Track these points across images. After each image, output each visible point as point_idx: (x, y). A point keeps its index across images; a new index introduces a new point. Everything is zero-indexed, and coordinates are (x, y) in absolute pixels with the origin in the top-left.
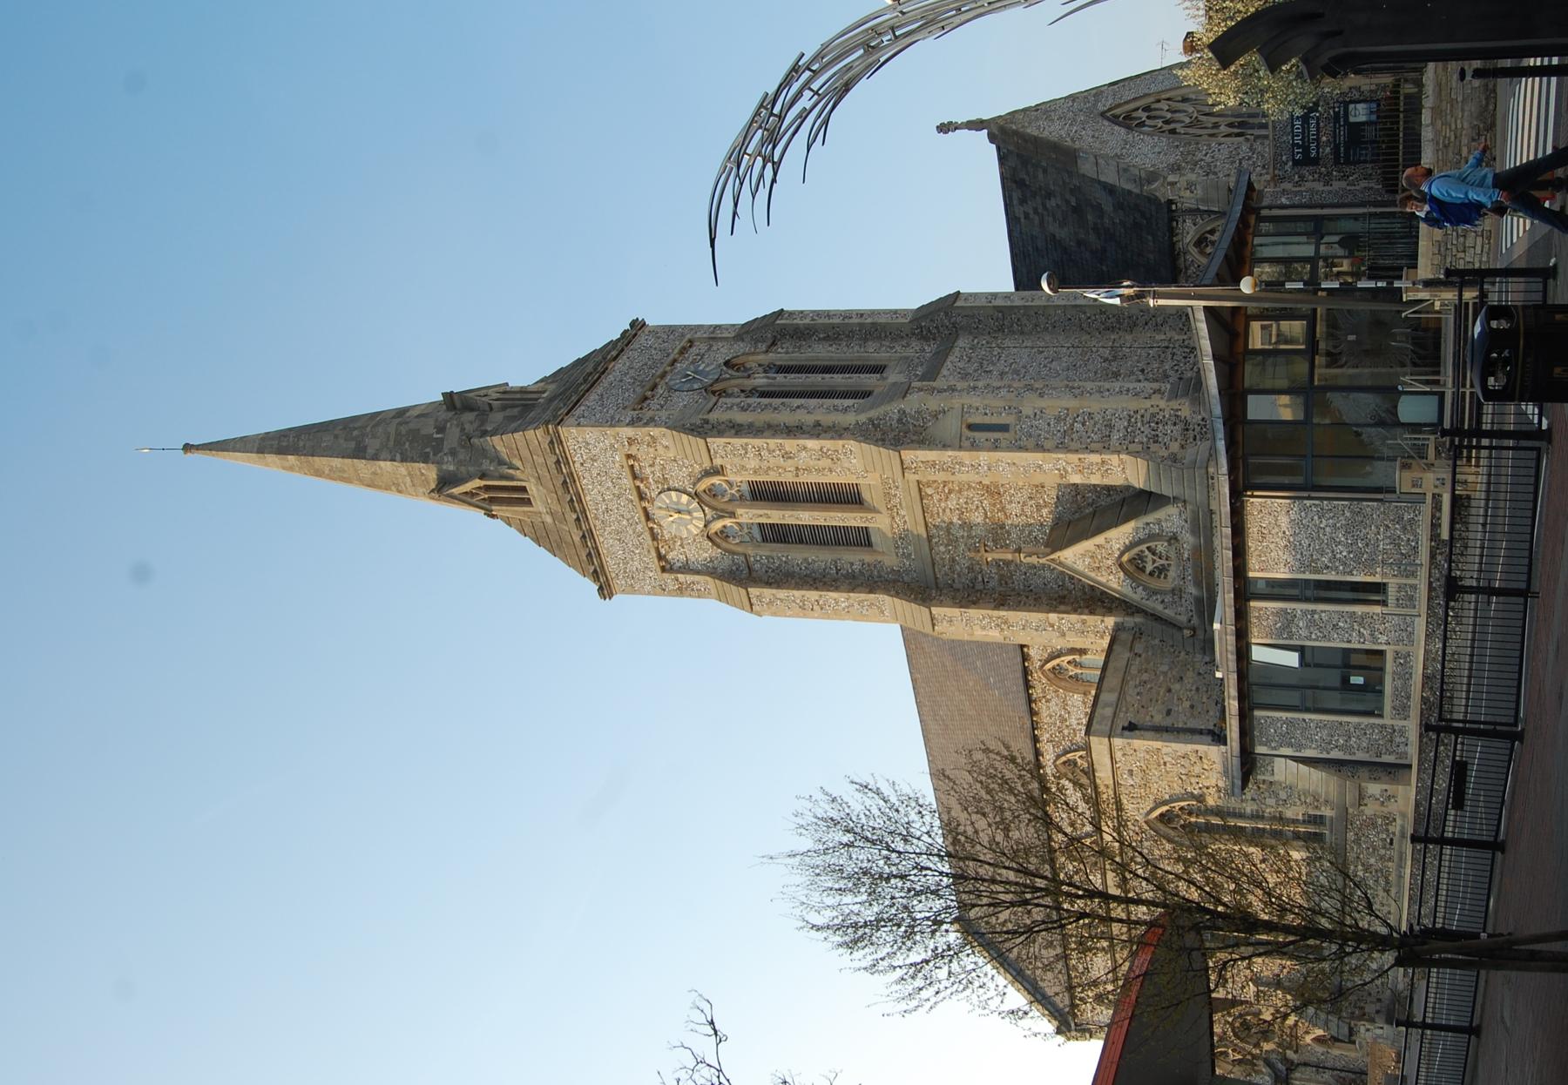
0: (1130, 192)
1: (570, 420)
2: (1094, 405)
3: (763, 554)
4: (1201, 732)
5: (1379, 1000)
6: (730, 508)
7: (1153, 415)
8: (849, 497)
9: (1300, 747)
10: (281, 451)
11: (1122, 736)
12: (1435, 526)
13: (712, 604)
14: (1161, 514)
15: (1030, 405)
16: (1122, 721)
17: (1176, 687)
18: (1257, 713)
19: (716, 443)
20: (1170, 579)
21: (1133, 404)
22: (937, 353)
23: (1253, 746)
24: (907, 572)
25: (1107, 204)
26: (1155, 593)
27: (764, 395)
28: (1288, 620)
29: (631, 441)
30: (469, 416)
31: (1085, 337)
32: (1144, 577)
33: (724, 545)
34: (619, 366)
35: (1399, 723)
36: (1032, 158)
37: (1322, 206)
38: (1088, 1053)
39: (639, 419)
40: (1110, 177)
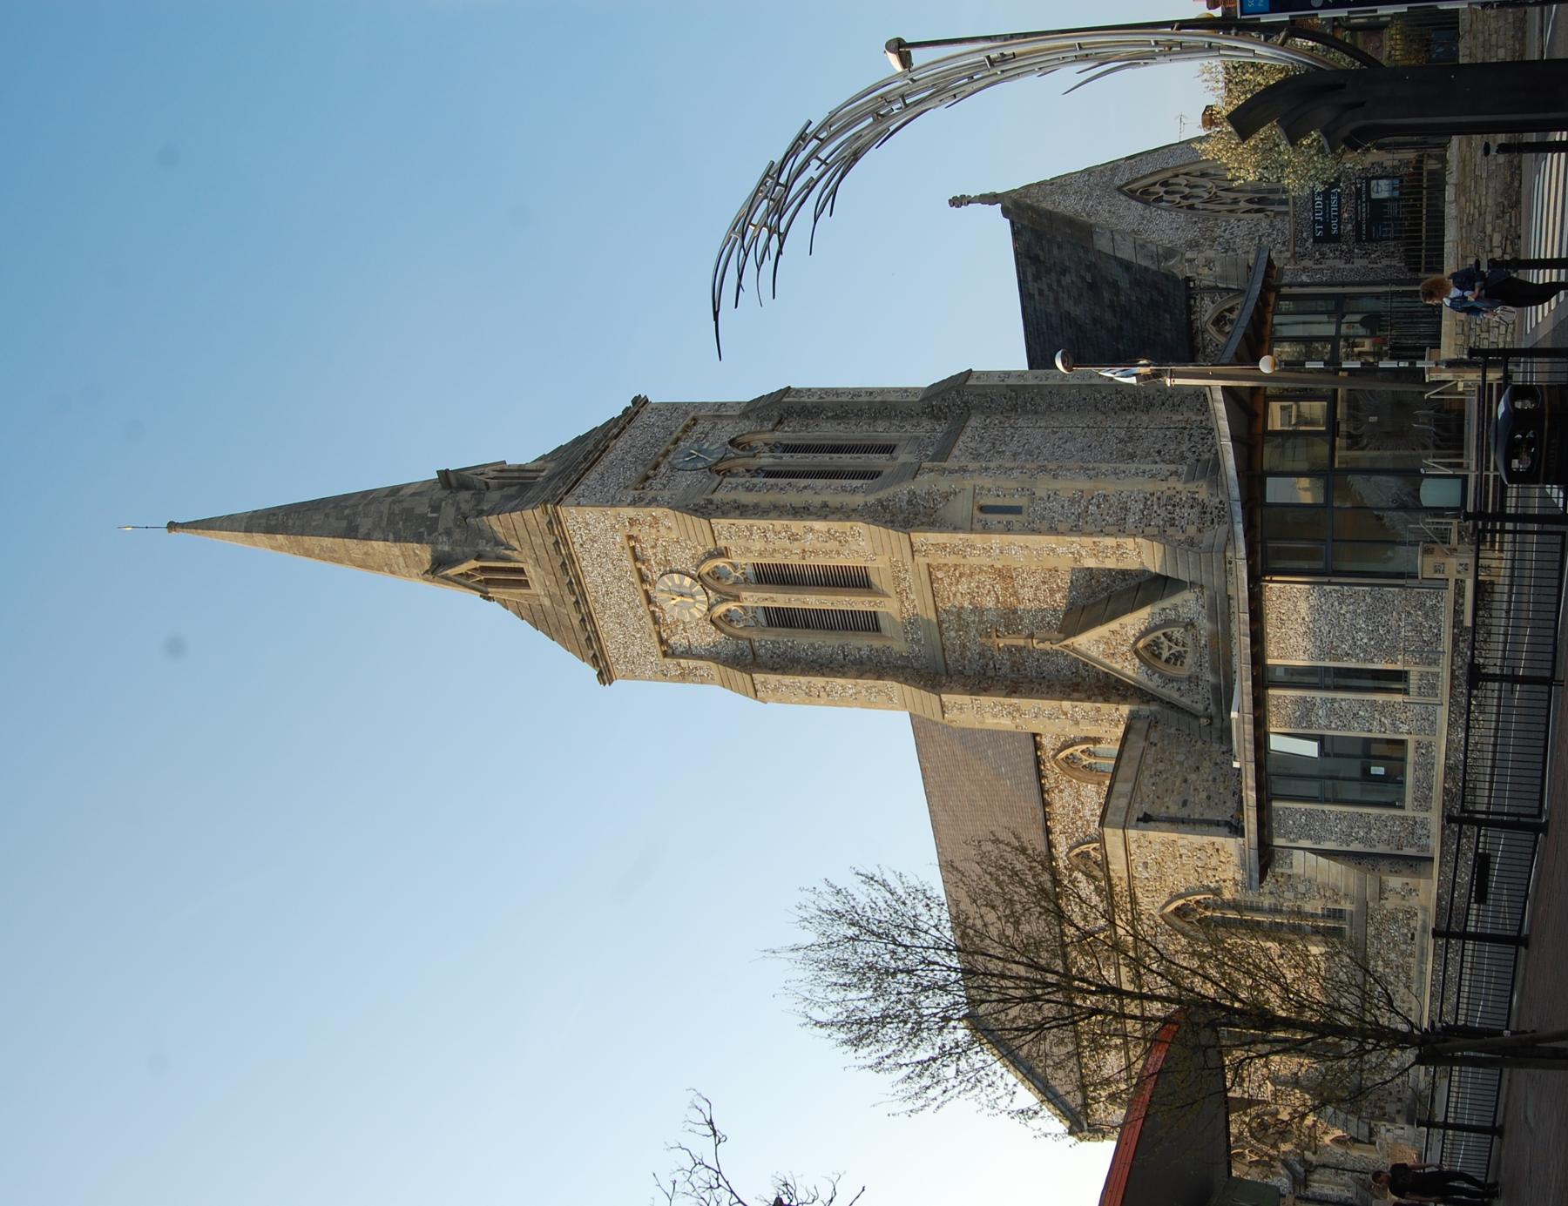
1: (569, 499)
2: (1108, 487)
3: (767, 639)
4: (1218, 824)
5: (1400, 1100)
6: (734, 591)
7: (1170, 498)
8: (857, 581)
9: (1319, 839)
11: (1136, 827)
12: (1458, 612)
14: (1177, 599)
15: (1044, 486)
17: (1192, 777)
18: (1275, 804)
19: (721, 524)
20: (1186, 666)
21: (1150, 487)
23: (1271, 836)
24: (917, 657)
26: (1171, 680)
27: (769, 474)
29: (632, 522)
31: (1100, 417)
32: (1160, 664)
33: (728, 629)
34: (620, 445)
35: (1420, 815)
36: (1047, 233)
37: (1343, 285)
39: (641, 499)
40: (1126, 253)
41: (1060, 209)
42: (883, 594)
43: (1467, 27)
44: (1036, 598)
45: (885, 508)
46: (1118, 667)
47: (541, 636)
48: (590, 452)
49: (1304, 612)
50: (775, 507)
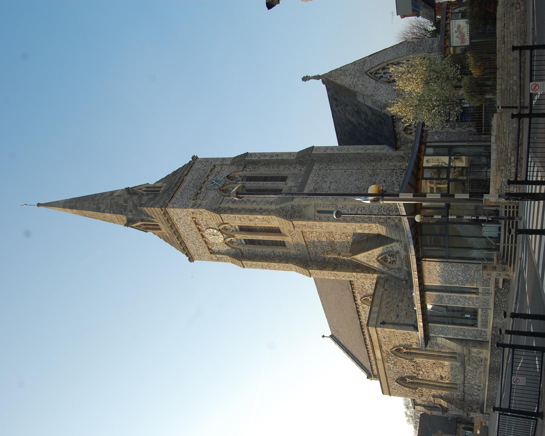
0: (377, 110)
1: (170, 205)
3: (247, 249)
4: (410, 325)
5: (478, 403)
6: (232, 234)
7: (388, 208)
8: (276, 231)
9: (446, 335)
10: (71, 208)
11: (380, 327)
13: (230, 264)
14: (393, 244)
16: (380, 321)
17: (400, 304)
18: (430, 324)
19: (224, 216)
22: (306, 172)
23: (429, 333)
24: (300, 255)
25: (369, 113)
26: (391, 269)
28: (441, 298)
29: (193, 213)
30: (135, 197)
31: (363, 164)
32: (387, 264)
33: (232, 245)
34: (188, 178)
35: (484, 329)
36: (340, 89)
37: (452, 142)
38: (437, 2)
39: (196, 205)
40: (369, 104)
41: (344, 83)
42: (286, 236)
43: (500, 65)
44: (341, 238)
45: (283, 210)
46: (372, 265)
47: (167, 244)
48: (177, 183)
49: (438, 270)
50: (243, 209)
